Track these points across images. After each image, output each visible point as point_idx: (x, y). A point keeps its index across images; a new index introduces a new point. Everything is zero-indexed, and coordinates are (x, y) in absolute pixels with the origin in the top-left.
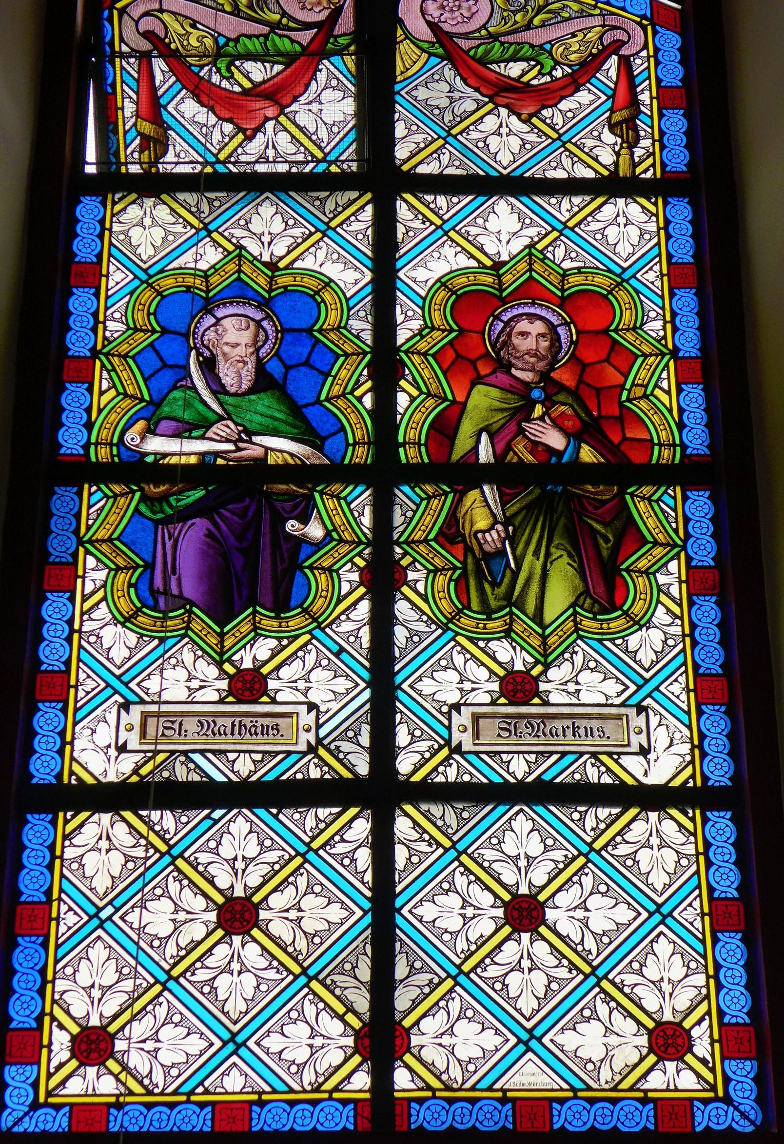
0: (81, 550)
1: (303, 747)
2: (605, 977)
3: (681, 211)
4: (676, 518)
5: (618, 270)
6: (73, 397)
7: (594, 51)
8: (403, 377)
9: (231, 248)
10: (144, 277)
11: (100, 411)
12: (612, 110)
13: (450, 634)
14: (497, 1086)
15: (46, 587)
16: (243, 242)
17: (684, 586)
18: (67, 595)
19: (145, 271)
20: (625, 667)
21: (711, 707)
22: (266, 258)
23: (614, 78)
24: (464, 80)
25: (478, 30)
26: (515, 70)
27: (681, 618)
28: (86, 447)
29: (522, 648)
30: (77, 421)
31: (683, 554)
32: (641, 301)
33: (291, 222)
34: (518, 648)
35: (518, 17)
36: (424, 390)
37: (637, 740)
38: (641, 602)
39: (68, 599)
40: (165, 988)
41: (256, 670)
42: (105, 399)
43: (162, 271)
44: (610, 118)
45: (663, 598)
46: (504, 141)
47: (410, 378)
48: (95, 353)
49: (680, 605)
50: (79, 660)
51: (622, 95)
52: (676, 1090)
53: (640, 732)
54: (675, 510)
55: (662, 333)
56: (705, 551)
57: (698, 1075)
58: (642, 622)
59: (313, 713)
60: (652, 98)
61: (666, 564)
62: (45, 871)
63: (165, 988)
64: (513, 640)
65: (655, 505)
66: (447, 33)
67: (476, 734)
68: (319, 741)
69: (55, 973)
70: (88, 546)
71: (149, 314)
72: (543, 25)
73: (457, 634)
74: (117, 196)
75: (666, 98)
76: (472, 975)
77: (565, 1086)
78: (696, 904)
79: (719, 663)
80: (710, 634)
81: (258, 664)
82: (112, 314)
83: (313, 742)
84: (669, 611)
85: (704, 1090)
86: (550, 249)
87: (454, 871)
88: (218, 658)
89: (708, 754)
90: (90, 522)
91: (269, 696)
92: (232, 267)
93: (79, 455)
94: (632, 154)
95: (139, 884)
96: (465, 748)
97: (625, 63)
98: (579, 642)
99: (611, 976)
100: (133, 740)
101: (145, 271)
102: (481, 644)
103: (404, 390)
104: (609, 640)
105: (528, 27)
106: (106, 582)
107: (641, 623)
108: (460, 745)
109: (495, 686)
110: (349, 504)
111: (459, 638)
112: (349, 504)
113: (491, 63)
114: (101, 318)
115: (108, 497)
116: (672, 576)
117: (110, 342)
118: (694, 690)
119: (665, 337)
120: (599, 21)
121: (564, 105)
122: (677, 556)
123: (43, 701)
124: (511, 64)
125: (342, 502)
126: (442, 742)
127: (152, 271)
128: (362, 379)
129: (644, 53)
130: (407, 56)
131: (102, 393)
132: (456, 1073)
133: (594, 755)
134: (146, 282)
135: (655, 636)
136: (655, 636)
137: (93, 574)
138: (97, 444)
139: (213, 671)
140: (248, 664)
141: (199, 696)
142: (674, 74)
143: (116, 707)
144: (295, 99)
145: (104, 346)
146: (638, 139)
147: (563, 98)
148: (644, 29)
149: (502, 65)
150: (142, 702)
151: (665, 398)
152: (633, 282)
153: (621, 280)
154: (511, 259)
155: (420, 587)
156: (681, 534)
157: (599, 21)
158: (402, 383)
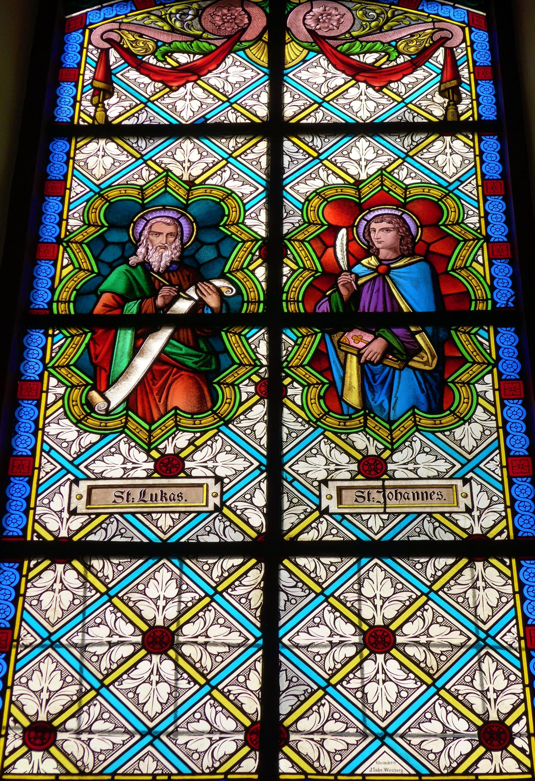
0: (46, 373)
1: (211, 508)
2: (443, 687)
3: (492, 144)
4: (490, 346)
5: (445, 184)
6: (44, 268)
7: (427, 45)
8: (286, 256)
9: (160, 170)
10: (97, 190)
11: (61, 281)
12: (441, 82)
13: (320, 430)
14: (359, 771)
15: (10, 473)
16: (170, 167)
17: (497, 393)
18: (60, 198)
19: (98, 186)
20: (454, 451)
21: (520, 479)
22: (186, 178)
23: (442, 63)
24: (334, 66)
25: (344, 34)
26: (370, 59)
27: (496, 415)
28: (50, 304)
29: (374, 439)
30: (18, 508)
31: (495, 370)
32: (462, 205)
33: (205, 154)
34: (371, 439)
35: (373, 24)
36: (301, 265)
37: (463, 502)
38: (465, 405)
39: (27, 482)
40: (99, 694)
41: (176, 455)
42: (65, 272)
43: (110, 186)
44: (440, 87)
45: (481, 401)
46: (363, 102)
47: (291, 257)
48: (59, 240)
49: (494, 406)
50: (22, 619)
51: (448, 73)
52: (501, 773)
53: (466, 496)
54: (489, 340)
55: (478, 225)
56: (512, 368)
57: (519, 762)
58: (466, 418)
59: (219, 485)
60: (470, 73)
61: (482, 378)
62: (11, 605)
63: (99, 694)
64: (367, 433)
65: (473, 336)
66: (321, 36)
67: (340, 501)
68: (223, 503)
69: (13, 680)
70: (51, 370)
71: (82, 405)
72: (391, 29)
73: (326, 430)
74: (33, 563)
75: (479, 73)
76: (339, 687)
77: (412, 772)
78: (514, 630)
79: (525, 447)
80: (518, 426)
81: (177, 451)
82: (74, 215)
83: (218, 504)
84: (485, 410)
85: (523, 773)
86: (396, 171)
87: (324, 609)
88: (146, 447)
89: (518, 513)
90: (53, 355)
91: (185, 473)
92: (161, 184)
93: (44, 309)
94: (456, 109)
95: (80, 617)
96: (331, 511)
97: (450, 53)
98: (417, 434)
99: (447, 687)
100: (81, 506)
101: (98, 186)
102: (343, 436)
103: (288, 266)
104: (441, 432)
105: (380, 29)
106: (64, 395)
107: (465, 419)
108: (327, 508)
109: (354, 467)
110: (247, 339)
111: (327, 433)
112: (247, 339)
113: (354, 55)
114: (65, 217)
115: (67, 338)
116: (487, 386)
117: (71, 233)
118: (507, 467)
119: (480, 228)
120: (431, 26)
121: (406, 80)
122: (491, 372)
123: (14, 477)
124: (368, 55)
125: (243, 338)
126: (314, 507)
127: (102, 186)
128: (255, 258)
129: (463, 45)
130: (292, 52)
131: (63, 268)
132: (325, 761)
133: (430, 514)
134: (98, 193)
135: (476, 429)
136: (476, 429)
137: (54, 389)
138: (58, 301)
139: (143, 456)
140: (170, 450)
141: (132, 474)
142: (484, 59)
143: (69, 483)
144: (210, 71)
145: (66, 236)
146: (460, 100)
147: (404, 76)
148: (463, 29)
149: (361, 56)
150: (89, 478)
151: (480, 269)
152: (456, 192)
153: (448, 190)
154: (368, 178)
155: (298, 400)
156: (494, 356)
157: (431, 26)
158: (285, 260)
